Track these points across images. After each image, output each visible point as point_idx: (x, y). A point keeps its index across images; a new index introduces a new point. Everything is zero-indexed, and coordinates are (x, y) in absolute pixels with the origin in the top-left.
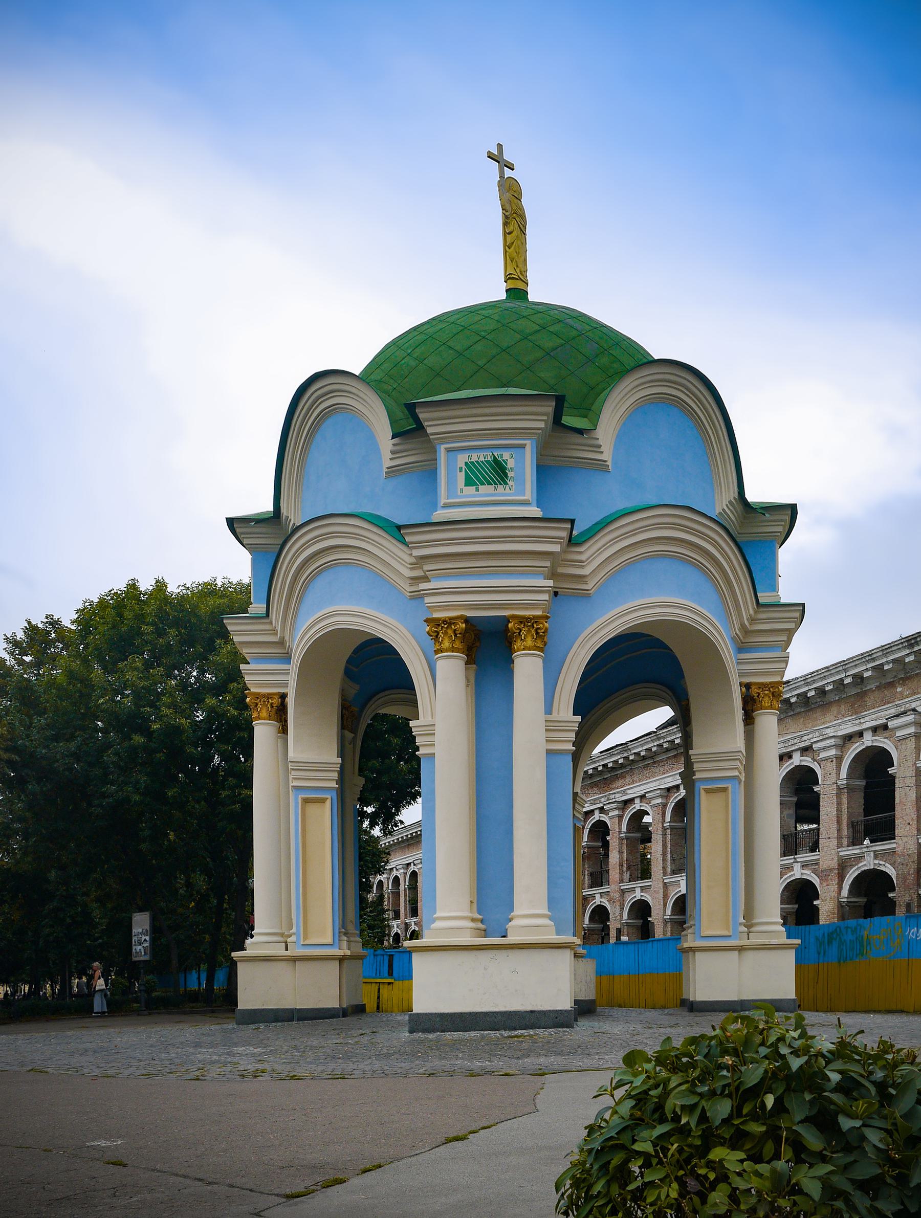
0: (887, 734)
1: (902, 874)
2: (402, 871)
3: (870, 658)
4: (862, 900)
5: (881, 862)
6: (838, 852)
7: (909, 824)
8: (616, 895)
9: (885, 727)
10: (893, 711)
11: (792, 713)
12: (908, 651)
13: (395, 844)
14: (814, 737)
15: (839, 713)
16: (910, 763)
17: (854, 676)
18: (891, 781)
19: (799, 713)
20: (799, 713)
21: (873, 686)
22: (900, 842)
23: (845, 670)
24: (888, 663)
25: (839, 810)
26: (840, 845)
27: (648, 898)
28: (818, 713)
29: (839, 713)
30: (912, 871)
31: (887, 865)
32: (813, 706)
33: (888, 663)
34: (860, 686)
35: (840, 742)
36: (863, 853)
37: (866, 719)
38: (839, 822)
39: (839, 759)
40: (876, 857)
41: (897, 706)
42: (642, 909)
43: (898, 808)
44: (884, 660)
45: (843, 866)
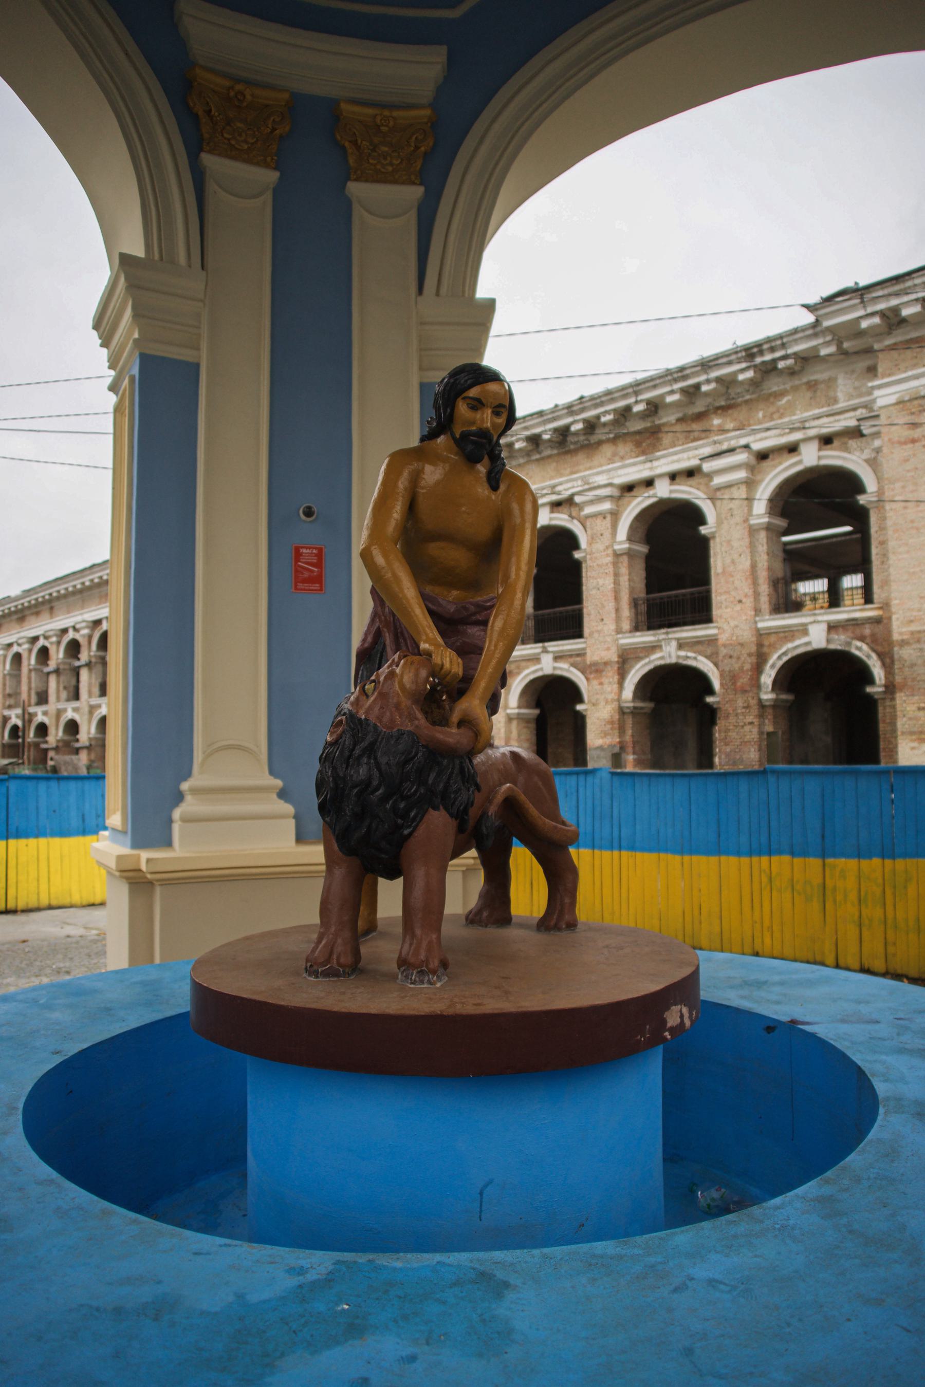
0: (694, 481)
1: (730, 671)
2: (86, 631)
3: (680, 374)
4: (649, 705)
5: (690, 654)
6: (617, 640)
7: (740, 601)
8: (86, 709)
9: (690, 473)
10: (707, 451)
11: (538, 456)
12: (744, 365)
13: (29, 607)
14: (577, 486)
15: (615, 454)
16: (738, 519)
17: (649, 402)
18: (576, 568)
19: (549, 457)
20: (549, 457)
21: (672, 418)
22: (725, 627)
23: (636, 393)
24: (708, 381)
25: (616, 583)
26: (757, 611)
27: (77, 717)
28: (581, 456)
29: (615, 454)
30: (747, 667)
31: (700, 658)
32: (572, 447)
33: (708, 381)
34: (650, 419)
35: (616, 493)
36: (659, 641)
37: (662, 461)
38: (617, 599)
39: (615, 515)
40: (680, 646)
41: (715, 443)
42: (72, 727)
43: (585, 603)
44: (703, 378)
45: (625, 660)
